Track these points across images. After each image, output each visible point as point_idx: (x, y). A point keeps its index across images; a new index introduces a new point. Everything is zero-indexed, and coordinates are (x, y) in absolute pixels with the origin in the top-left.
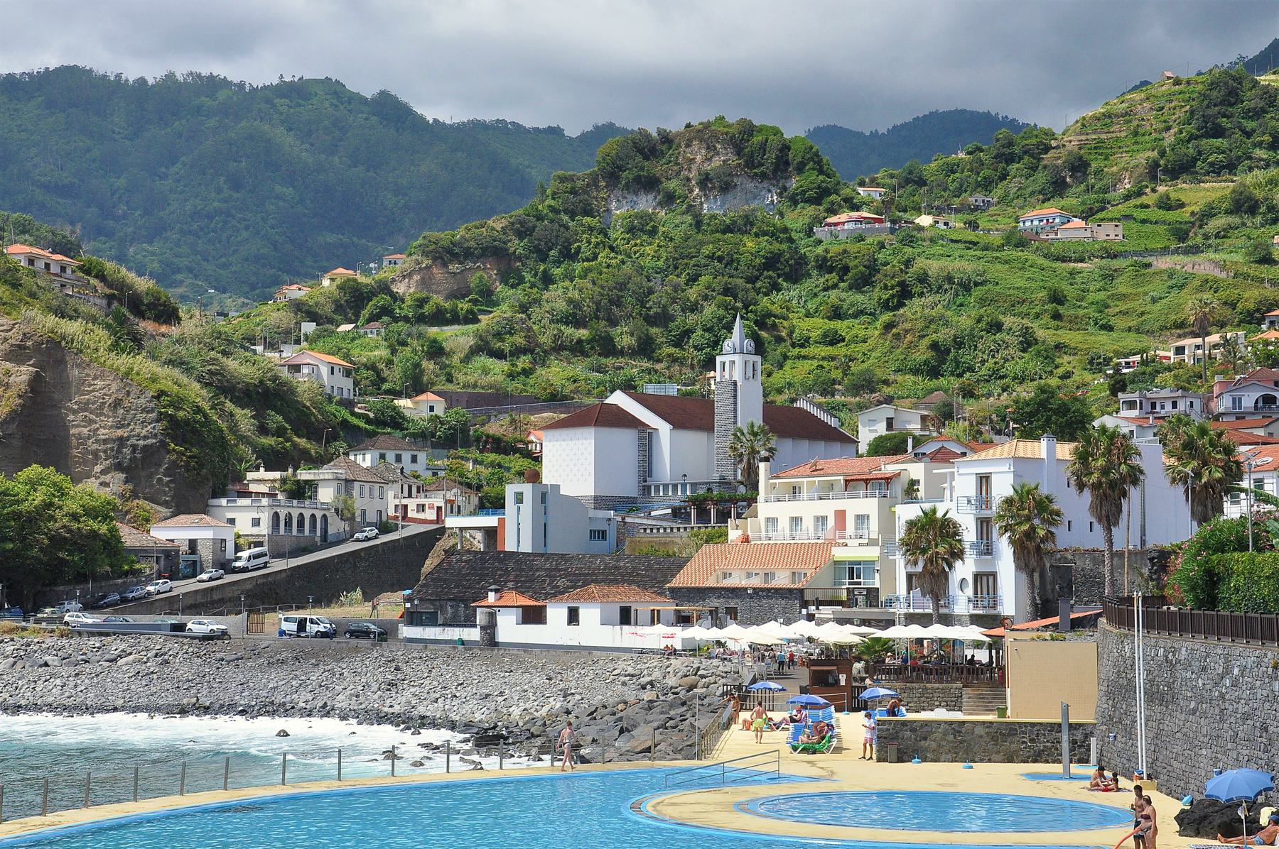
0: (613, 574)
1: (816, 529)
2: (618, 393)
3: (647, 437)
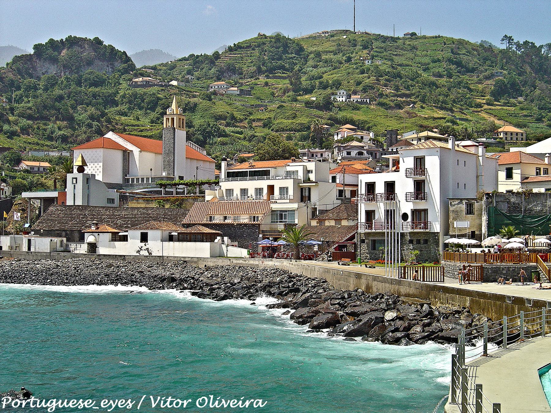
0: (146, 217)
1: (256, 195)
2: (111, 133)
3: (127, 154)
